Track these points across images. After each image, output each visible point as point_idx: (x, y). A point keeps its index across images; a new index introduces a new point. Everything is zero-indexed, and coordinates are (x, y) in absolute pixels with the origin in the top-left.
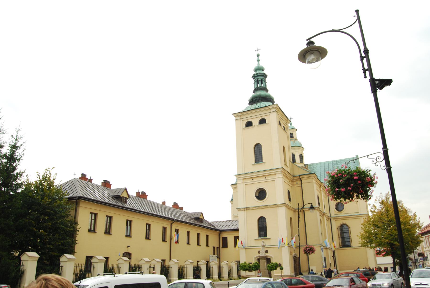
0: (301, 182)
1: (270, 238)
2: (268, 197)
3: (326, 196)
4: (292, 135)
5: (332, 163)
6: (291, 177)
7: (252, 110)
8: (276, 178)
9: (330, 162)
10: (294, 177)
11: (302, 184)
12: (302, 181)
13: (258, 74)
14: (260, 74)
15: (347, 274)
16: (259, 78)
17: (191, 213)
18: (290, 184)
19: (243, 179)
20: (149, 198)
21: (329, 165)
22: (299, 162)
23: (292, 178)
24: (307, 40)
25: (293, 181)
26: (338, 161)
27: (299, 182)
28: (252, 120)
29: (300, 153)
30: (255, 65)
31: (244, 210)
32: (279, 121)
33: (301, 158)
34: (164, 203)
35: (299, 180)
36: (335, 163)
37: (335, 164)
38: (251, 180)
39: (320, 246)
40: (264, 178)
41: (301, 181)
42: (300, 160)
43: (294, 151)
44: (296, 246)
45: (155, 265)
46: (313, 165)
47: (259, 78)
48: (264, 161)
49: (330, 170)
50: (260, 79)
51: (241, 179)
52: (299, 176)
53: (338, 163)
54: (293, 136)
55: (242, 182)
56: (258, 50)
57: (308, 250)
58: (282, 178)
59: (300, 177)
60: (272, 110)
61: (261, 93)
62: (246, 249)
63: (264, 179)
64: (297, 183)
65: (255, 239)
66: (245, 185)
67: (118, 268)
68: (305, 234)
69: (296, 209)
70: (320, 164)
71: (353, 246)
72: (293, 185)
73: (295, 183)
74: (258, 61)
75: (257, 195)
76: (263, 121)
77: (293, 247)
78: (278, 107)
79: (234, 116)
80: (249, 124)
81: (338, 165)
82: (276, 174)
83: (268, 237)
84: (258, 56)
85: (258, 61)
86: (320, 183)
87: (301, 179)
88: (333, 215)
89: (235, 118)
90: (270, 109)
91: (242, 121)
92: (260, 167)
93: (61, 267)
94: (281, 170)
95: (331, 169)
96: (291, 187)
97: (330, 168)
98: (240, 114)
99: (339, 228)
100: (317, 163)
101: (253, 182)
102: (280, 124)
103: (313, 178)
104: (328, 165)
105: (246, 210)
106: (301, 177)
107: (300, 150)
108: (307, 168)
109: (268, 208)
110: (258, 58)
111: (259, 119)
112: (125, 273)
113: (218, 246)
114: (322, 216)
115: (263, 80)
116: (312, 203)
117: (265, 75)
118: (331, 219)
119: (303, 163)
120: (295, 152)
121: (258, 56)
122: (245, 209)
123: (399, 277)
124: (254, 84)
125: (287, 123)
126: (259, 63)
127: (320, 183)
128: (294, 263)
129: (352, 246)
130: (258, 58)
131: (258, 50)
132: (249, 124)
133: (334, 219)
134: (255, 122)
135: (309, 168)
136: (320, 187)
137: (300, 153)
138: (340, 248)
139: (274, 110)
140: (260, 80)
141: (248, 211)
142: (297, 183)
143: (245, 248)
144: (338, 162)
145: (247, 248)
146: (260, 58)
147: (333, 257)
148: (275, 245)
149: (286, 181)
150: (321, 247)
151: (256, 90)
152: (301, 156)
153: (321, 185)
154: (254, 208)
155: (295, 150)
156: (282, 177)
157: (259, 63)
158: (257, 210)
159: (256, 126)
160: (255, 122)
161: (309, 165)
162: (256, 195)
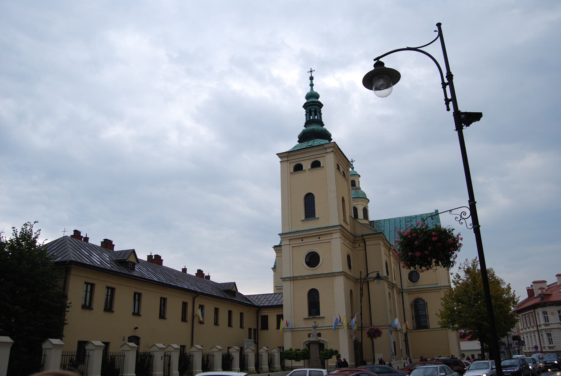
0: (365, 244)
1: (324, 317)
5: (404, 219)
6: (352, 237)
9: (402, 218)
11: (366, 247)
14: (313, 103)
16: (312, 108)
19: (289, 239)
24: (375, 60)
27: (362, 244)
28: (303, 163)
30: (308, 90)
31: (291, 280)
32: (338, 165)
36: (409, 219)
37: (408, 221)
38: (300, 241)
39: (388, 327)
40: (317, 239)
41: (365, 242)
42: (364, 216)
43: (356, 203)
45: (125, 352)
46: (380, 222)
48: (317, 216)
51: (287, 240)
52: (363, 236)
55: (288, 243)
56: (311, 71)
57: (373, 332)
59: (363, 238)
60: (328, 150)
62: (292, 331)
64: (359, 245)
65: (304, 319)
67: (121, 357)
71: (430, 328)
73: (357, 245)
74: (312, 85)
75: (308, 261)
76: (316, 165)
78: (337, 146)
80: (298, 168)
81: (412, 223)
83: (321, 315)
84: (312, 78)
85: (312, 85)
86: (389, 245)
87: (364, 240)
88: (405, 287)
89: (279, 160)
90: (326, 149)
92: (311, 224)
93: (43, 357)
97: (402, 226)
98: (287, 155)
99: (413, 304)
100: (386, 220)
102: (338, 168)
104: (399, 223)
106: (364, 237)
109: (322, 277)
111: (311, 161)
113: (256, 328)
115: (318, 110)
116: (378, 272)
118: (402, 293)
121: (312, 78)
122: (292, 279)
124: (305, 115)
125: (347, 167)
126: (312, 89)
129: (429, 328)
131: (311, 71)
132: (298, 168)
133: (406, 292)
134: (307, 165)
135: (375, 226)
136: (389, 251)
138: (414, 329)
140: (313, 111)
141: (295, 282)
142: (359, 245)
145: (293, 330)
147: (405, 342)
154: (303, 278)
155: (358, 202)
156: (340, 237)
157: (312, 89)
159: (307, 170)
160: (307, 165)
162: (306, 261)
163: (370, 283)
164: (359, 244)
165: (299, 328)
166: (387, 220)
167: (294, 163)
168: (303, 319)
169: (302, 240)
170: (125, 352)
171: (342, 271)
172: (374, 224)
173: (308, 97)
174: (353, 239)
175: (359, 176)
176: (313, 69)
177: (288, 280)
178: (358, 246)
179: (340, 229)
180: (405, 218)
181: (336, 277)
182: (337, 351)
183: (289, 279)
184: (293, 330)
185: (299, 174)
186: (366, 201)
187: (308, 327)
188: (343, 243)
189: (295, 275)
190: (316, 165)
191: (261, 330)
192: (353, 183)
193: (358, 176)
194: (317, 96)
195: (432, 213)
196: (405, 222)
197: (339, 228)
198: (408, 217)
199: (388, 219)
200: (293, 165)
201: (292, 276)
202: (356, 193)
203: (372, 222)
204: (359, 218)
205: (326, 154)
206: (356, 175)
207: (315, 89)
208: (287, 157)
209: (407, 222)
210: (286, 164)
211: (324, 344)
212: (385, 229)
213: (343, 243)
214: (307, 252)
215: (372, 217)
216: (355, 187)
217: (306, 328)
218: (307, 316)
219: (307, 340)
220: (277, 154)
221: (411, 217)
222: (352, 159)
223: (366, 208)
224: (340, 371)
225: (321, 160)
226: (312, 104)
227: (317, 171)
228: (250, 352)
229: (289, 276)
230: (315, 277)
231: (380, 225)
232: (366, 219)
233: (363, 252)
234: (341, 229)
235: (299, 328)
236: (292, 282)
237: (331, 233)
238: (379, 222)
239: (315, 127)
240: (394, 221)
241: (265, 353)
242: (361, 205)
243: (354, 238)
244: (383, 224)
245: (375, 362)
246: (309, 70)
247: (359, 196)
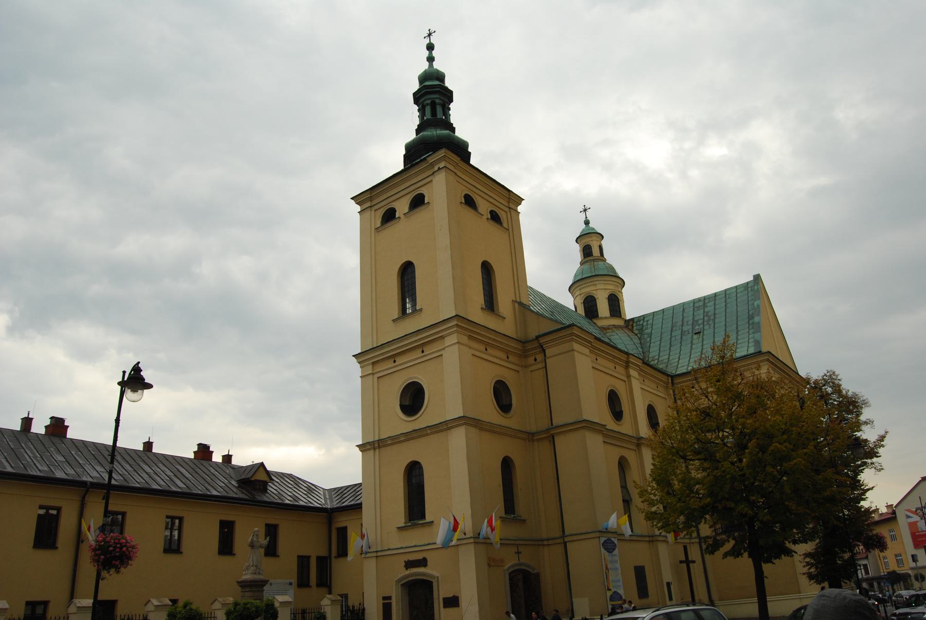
1: (432, 522)
2: (428, 404)
4: (589, 249)
5: (692, 304)
6: (519, 346)
7: (394, 179)
8: (444, 349)
9: (688, 303)
10: (526, 345)
14: (426, 89)
16: (424, 101)
17: (217, 464)
18: (514, 364)
19: (373, 364)
20: (70, 434)
21: (686, 311)
22: (608, 314)
23: (521, 348)
25: (526, 357)
26: (709, 298)
29: (609, 291)
30: (425, 66)
31: (375, 449)
34: (148, 445)
35: (539, 350)
36: (701, 303)
37: (699, 308)
38: (390, 364)
39: (597, 534)
41: (544, 351)
43: (593, 288)
44: (500, 539)
45: (216, 611)
46: (646, 319)
47: (424, 101)
49: (685, 324)
51: (368, 365)
52: (537, 337)
53: (708, 304)
54: (592, 252)
55: (371, 372)
58: (457, 346)
62: (376, 556)
63: (419, 356)
64: (535, 360)
65: (398, 528)
66: (378, 378)
68: (558, 503)
69: (533, 432)
70: (663, 312)
73: (531, 360)
74: (431, 59)
77: (492, 544)
79: (357, 203)
80: (389, 216)
81: (706, 310)
82: (444, 338)
84: (430, 47)
85: (431, 59)
86: (626, 356)
89: (358, 208)
91: (373, 211)
92: (411, 325)
94: (454, 322)
95: (687, 321)
96: (518, 371)
97: (685, 320)
98: (369, 196)
100: (656, 312)
101: (394, 367)
103: (572, 340)
104: (681, 313)
105: (379, 447)
106: (542, 340)
107: (608, 284)
108: (630, 329)
109: (427, 435)
110: (431, 53)
112: (506, 616)
113: (323, 553)
114: (634, 447)
117: (441, 88)
119: (620, 316)
121: (430, 47)
122: (376, 445)
125: (509, 202)
126: (431, 65)
127: (624, 357)
128: (512, 592)
130: (431, 53)
132: (389, 216)
134: (402, 207)
135: (635, 328)
137: (609, 291)
139: (442, 165)
141: (383, 450)
142: (535, 360)
143: (375, 554)
144: (706, 301)
145: (379, 554)
146: (434, 53)
149: (617, 373)
150: (599, 537)
153: (627, 362)
154: (395, 440)
155: (595, 285)
156: (458, 343)
157: (431, 65)
158: (404, 444)
159: (402, 216)
160: (402, 207)
161: (635, 320)
162: (403, 404)
163: (555, 438)
165: (389, 549)
166: (659, 313)
168: (396, 529)
169: (395, 362)
170: (216, 611)
171: (462, 415)
172: (635, 324)
173: (423, 78)
174: (521, 348)
175: (601, 238)
176: (432, 30)
177: (369, 449)
178: (534, 362)
179: (457, 325)
180: (694, 302)
181: (452, 430)
182: (456, 597)
183: (371, 445)
184: (379, 555)
185: (394, 229)
186: (615, 282)
187: (404, 546)
189: (382, 437)
190: (418, 202)
191: (335, 557)
192: (588, 251)
193: (598, 235)
194: (440, 77)
195: (747, 282)
196: (694, 310)
197: (454, 322)
198: (699, 300)
199: (661, 310)
200: (380, 213)
201: (377, 439)
202: (591, 268)
203: (630, 324)
204: (600, 316)
205: (432, 176)
206: (592, 235)
207: (437, 65)
208: (371, 199)
209: (696, 309)
210: (367, 214)
211: (432, 582)
212: (653, 331)
214: (403, 384)
215: (631, 311)
216: (591, 258)
217: (402, 548)
218: (403, 521)
219: (403, 575)
220: (351, 199)
221: (705, 298)
222: (584, 206)
225: (425, 191)
227: (421, 214)
228: (219, 609)
229: (372, 440)
230: (415, 435)
231: (645, 324)
232: (619, 317)
233: (542, 372)
234: (460, 324)
235: (389, 549)
236: (377, 450)
237: (442, 337)
238: (643, 319)
240: (672, 312)
241: (330, 607)
242: (604, 290)
244: (650, 322)
245: (573, 617)
246: (426, 33)
247: (597, 273)
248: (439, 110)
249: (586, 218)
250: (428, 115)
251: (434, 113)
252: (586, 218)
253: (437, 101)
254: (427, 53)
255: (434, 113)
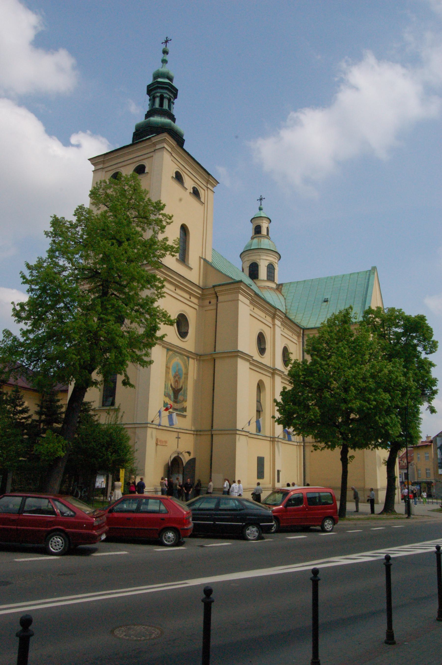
0: (217, 301)
3: (299, 342)
10: (204, 291)
11: (218, 304)
12: (219, 298)
13: (156, 84)
15: (21, 498)
16: (155, 93)
22: (265, 278)
25: (203, 299)
27: (214, 301)
33: (270, 272)
41: (217, 297)
42: (268, 276)
50: (158, 95)
52: (214, 287)
61: (157, 119)
64: (210, 303)
72: (202, 307)
73: (207, 302)
84: (165, 52)
86: (274, 310)
87: (216, 293)
89: (93, 168)
91: (104, 172)
106: (217, 289)
111: (133, 167)
120: (258, 260)
123: (110, 515)
136: (273, 318)
140: (158, 97)
142: (210, 303)
148: (222, 430)
151: (149, 115)
152: (271, 268)
164: (208, 301)
167: (112, 171)
188: (281, 334)
208: (103, 162)
213: (281, 334)
220: (89, 160)
223: (272, 265)
224: (56, 498)
226: (158, 86)
239: (157, 119)
243: (202, 292)
248: (166, 102)
249: (261, 205)
250: (157, 105)
251: (161, 104)
252: (261, 205)
253: (165, 95)
254: (161, 56)
255: (161, 104)
